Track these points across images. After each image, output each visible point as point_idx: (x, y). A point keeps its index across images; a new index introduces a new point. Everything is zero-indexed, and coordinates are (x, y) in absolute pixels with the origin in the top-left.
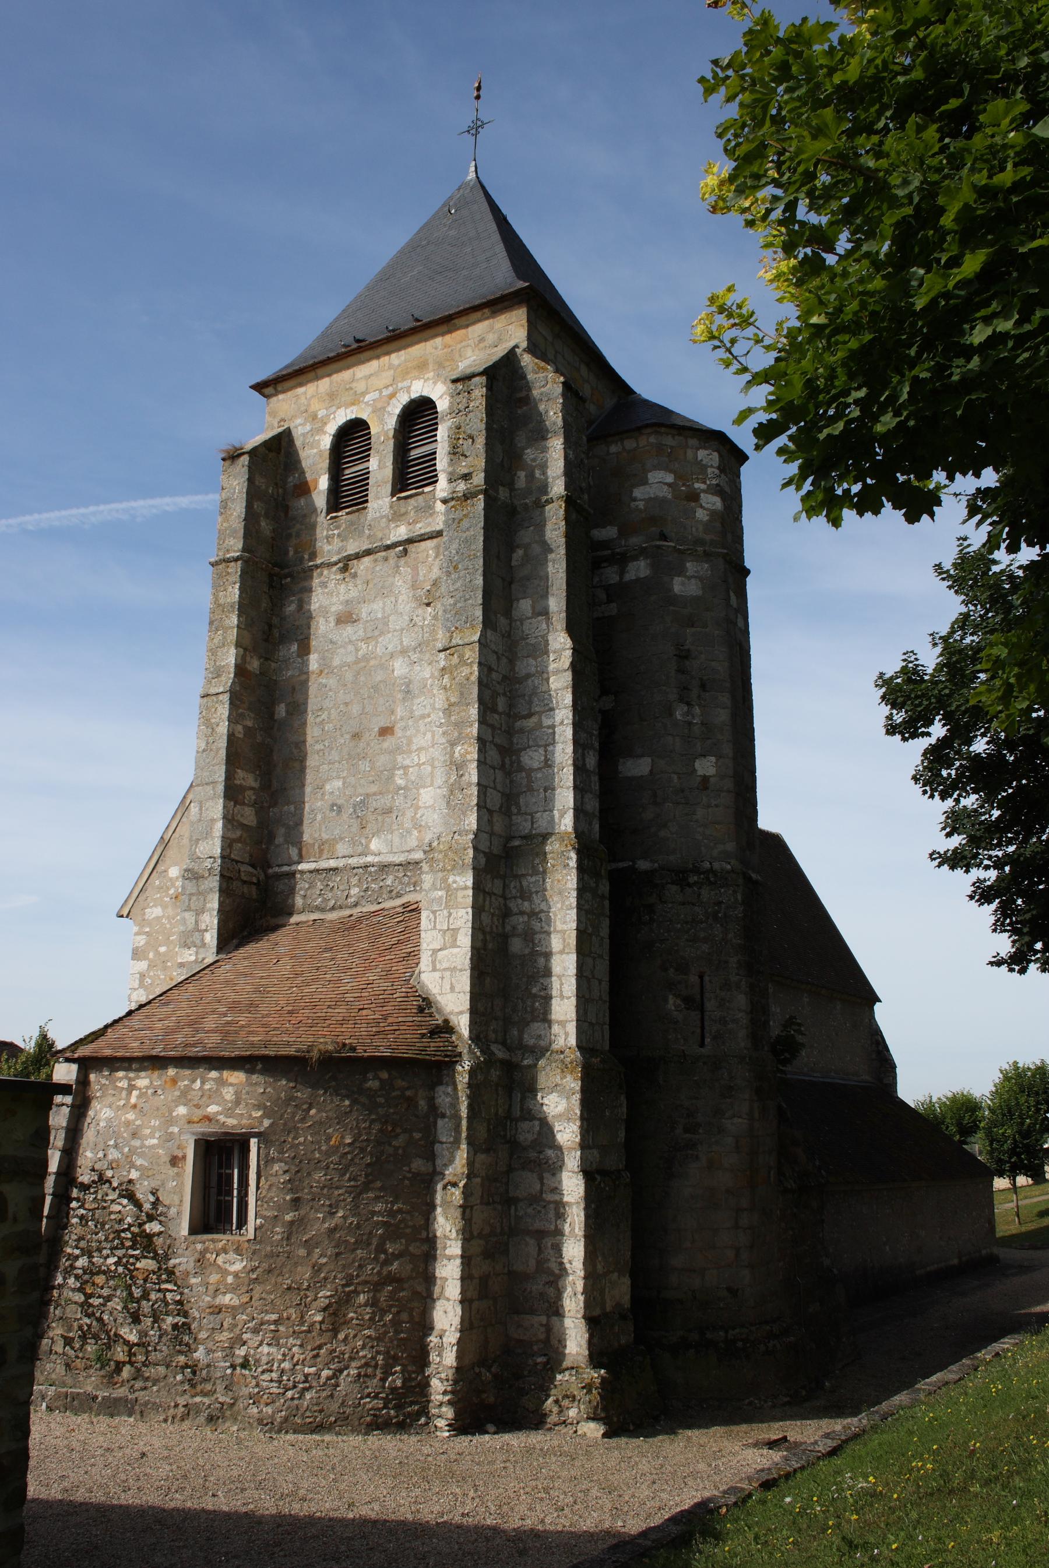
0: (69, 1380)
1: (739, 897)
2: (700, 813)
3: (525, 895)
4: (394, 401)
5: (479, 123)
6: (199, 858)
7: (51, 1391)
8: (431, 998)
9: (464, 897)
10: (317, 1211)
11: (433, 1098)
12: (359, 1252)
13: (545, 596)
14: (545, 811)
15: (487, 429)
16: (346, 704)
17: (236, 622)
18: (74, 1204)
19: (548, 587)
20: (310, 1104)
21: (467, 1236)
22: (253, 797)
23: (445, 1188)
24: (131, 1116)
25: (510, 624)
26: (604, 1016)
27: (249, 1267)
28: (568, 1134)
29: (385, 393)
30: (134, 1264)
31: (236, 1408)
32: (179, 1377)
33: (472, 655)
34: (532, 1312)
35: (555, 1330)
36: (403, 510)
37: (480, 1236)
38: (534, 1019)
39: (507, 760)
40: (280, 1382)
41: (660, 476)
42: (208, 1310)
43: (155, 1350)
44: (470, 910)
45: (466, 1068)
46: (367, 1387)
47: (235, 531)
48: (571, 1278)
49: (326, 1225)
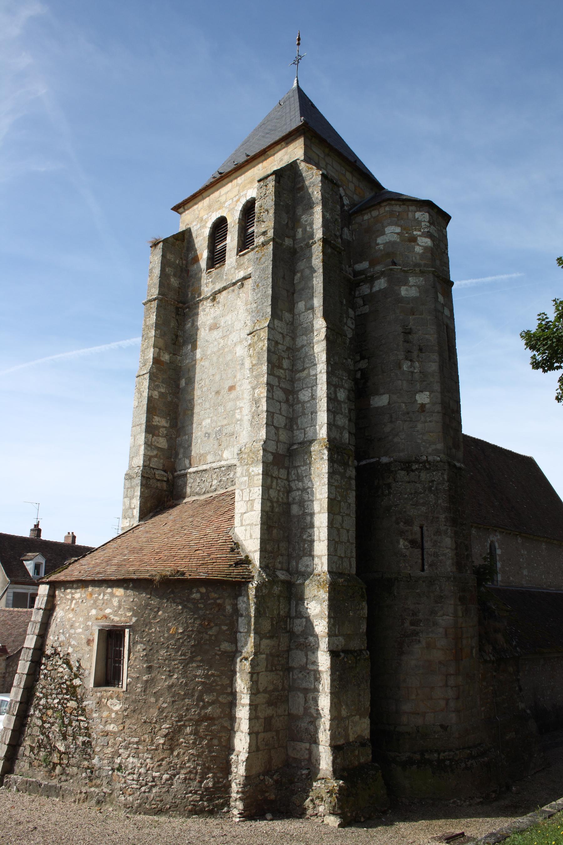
0: (31, 773)
1: (446, 477)
2: (420, 426)
3: (300, 478)
4: (239, 203)
5: (299, 57)
6: (133, 467)
7: (20, 779)
8: (240, 543)
9: (257, 480)
10: (162, 674)
11: (236, 604)
12: (186, 700)
13: (312, 297)
14: (311, 426)
15: (275, 205)
16: (213, 375)
17: (154, 334)
18: (43, 667)
19: (313, 293)
20: (159, 608)
21: (254, 692)
22: (165, 432)
23: (241, 661)
24: (71, 615)
25: (293, 317)
26: (351, 552)
27: (123, 708)
28: (321, 627)
29: (235, 199)
30: (66, 704)
31: (112, 796)
32: (84, 775)
33: (264, 334)
34: (301, 740)
35: (314, 753)
36: (242, 262)
37: (265, 691)
38: (304, 555)
39: (290, 397)
40: (138, 781)
41: (392, 229)
42: (101, 734)
43: (73, 757)
44: (261, 488)
45: (254, 585)
46: (190, 787)
47: (155, 284)
48: (323, 720)
49: (167, 683)
